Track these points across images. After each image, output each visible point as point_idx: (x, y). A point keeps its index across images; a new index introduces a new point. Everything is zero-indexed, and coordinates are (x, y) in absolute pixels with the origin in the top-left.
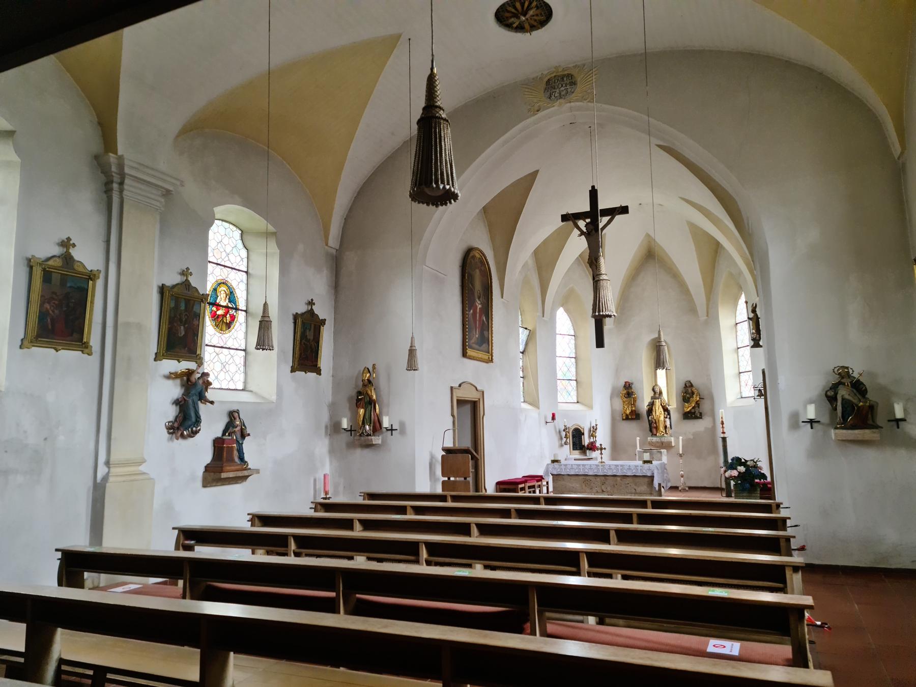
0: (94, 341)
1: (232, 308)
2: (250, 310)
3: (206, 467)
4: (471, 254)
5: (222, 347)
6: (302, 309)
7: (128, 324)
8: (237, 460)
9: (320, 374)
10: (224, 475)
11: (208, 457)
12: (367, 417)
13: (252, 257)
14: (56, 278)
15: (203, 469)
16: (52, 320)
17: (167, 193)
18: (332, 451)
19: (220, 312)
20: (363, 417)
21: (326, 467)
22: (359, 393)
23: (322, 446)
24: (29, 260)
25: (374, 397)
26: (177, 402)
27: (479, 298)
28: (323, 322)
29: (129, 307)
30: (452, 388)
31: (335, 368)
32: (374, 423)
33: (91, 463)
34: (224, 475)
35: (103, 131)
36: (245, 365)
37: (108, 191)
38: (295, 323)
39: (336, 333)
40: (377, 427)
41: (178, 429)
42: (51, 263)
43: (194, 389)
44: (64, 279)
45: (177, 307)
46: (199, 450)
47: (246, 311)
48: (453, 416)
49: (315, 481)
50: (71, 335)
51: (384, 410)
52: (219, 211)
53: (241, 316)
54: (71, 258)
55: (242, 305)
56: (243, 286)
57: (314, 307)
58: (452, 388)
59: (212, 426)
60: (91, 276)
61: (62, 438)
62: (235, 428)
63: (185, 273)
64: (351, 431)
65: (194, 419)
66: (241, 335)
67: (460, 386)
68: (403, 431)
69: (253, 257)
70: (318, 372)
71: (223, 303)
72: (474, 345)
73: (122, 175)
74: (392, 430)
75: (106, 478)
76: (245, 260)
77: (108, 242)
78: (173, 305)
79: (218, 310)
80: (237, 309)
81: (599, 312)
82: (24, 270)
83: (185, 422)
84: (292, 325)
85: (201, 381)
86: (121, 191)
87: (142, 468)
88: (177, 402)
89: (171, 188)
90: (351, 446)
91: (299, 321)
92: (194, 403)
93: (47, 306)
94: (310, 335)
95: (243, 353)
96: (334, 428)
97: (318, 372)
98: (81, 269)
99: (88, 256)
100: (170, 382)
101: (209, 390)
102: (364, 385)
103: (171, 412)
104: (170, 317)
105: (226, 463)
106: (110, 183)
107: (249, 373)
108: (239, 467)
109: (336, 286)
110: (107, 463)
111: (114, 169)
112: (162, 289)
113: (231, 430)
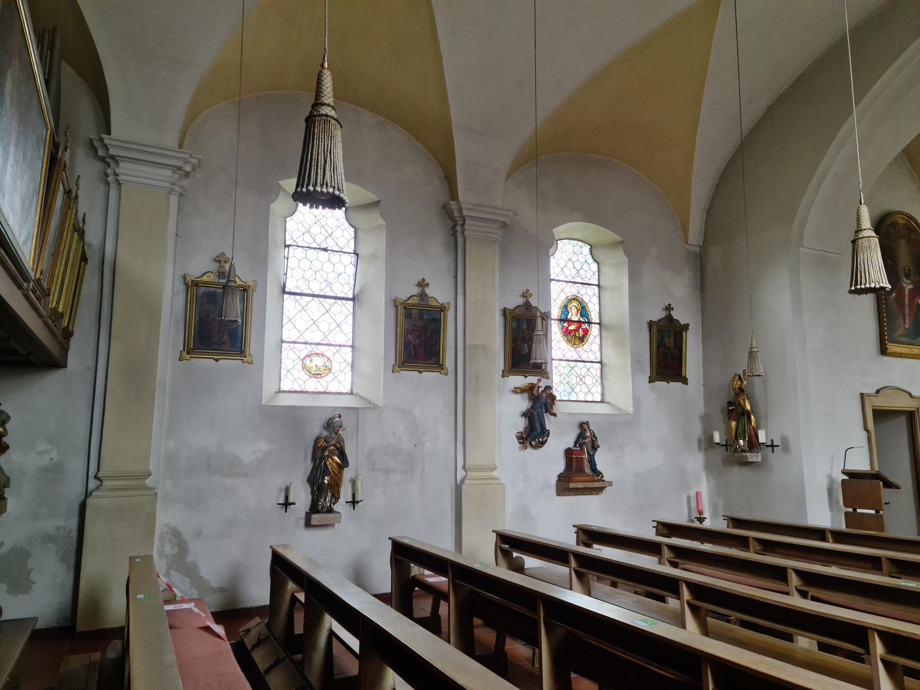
0: (449, 363)
1: (585, 322)
2: (603, 323)
3: (559, 476)
4: (889, 221)
5: (576, 361)
6: (657, 315)
7: (474, 346)
8: (588, 470)
9: (687, 384)
10: (572, 485)
11: (560, 467)
12: (740, 430)
13: (603, 270)
14: (414, 312)
15: (556, 478)
16: (414, 348)
17: (504, 225)
18: (708, 467)
19: (572, 328)
20: (738, 431)
21: (703, 486)
22: (730, 403)
23: (695, 462)
24: (395, 301)
25: (748, 407)
26: (524, 415)
27: (907, 277)
28: (686, 327)
29: (477, 332)
30: (862, 395)
31: (707, 376)
32: (750, 437)
33: (453, 467)
34: (572, 485)
35: (449, 183)
36: (601, 377)
37: (454, 234)
38: (650, 331)
39: (706, 338)
40: (754, 444)
41: (526, 439)
42: (410, 301)
43: (541, 404)
44: (421, 313)
45: (519, 326)
46: (551, 459)
47: (599, 324)
48: (866, 429)
49: (689, 498)
50: (430, 359)
51: (762, 422)
52: (558, 231)
53: (595, 330)
54: (426, 295)
55: (595, 317)
56: (595, 300)
57: (672, 313)
58: (862, 395)
59: (561, 439)
60: (442, 309)
61: (428, 444)
62: (585, 444)
63: (526, 295)
64: (726, 445)
65: (539, 430)
66: (596, 347)
67: (878, 391)
68: (786, 448)
69: (604, 270)
70: (685, 381)
71: (575, 318)
72: (903, 339)
73: (464, 218)
74: (772, 446)
75: (463, 481)
76: (597, 273)
77: (456, 277)
78: (515, 325)
79: (569, 325)
80: (590, 323)
81: (856, 284)
82: (393, 309)
83: (533, 434)
84: (648, 333)
85: (544, 395)
86: (463, 231)
87: (495, 474)
88: (524, 415)
89: (505, 219)
90: (729, 462)
91: (655, 329)
92: (538, 414)
93: (410, 337)
94: (669, 342)
95: (599, 365)
96: (707, 443)
97: (685, 381)
98: (435, 304)
99: (439, 293)
100: (518, 396)
101: (556, 403)
102: (737, 395)
103: (521, 424)
104: (513, 337)
105: (579, 473)
106: (454, 225)
107: (606, 385)
108: (589, 478)
109: (702, 286)
110: (464, 467)
111: (456, 214)
112: (505, 312)
113: (581, 441)
